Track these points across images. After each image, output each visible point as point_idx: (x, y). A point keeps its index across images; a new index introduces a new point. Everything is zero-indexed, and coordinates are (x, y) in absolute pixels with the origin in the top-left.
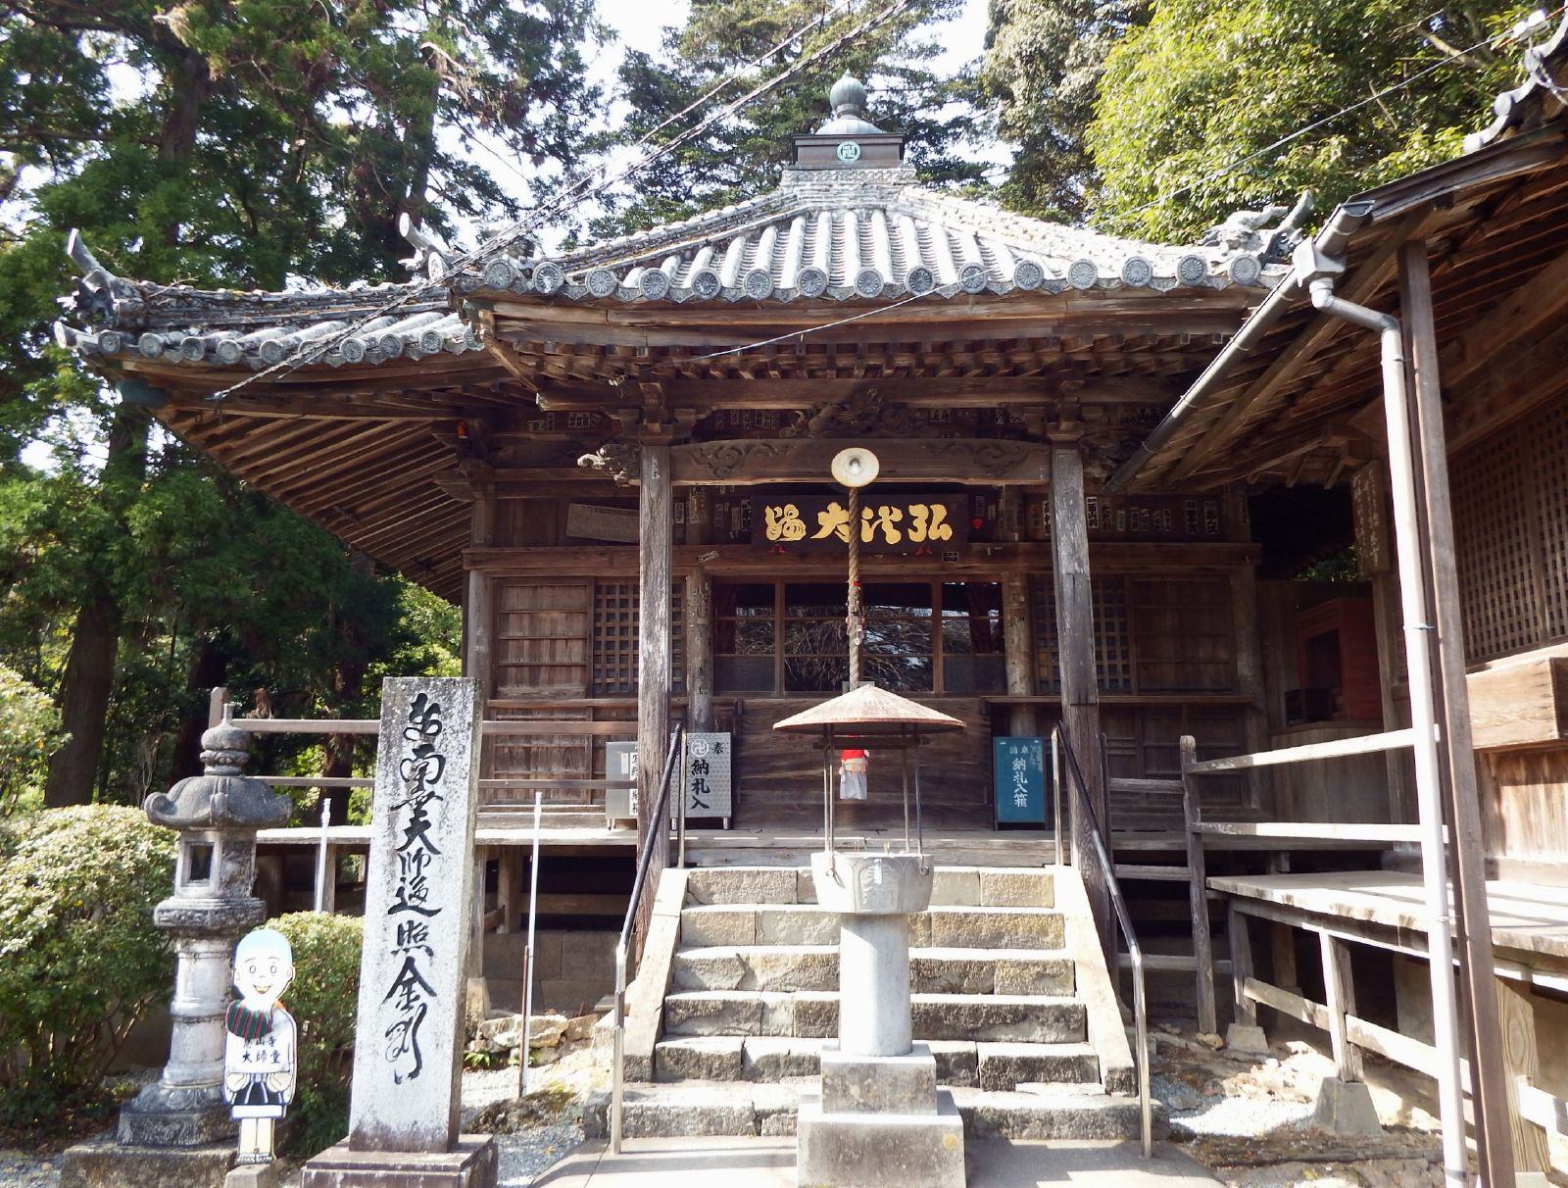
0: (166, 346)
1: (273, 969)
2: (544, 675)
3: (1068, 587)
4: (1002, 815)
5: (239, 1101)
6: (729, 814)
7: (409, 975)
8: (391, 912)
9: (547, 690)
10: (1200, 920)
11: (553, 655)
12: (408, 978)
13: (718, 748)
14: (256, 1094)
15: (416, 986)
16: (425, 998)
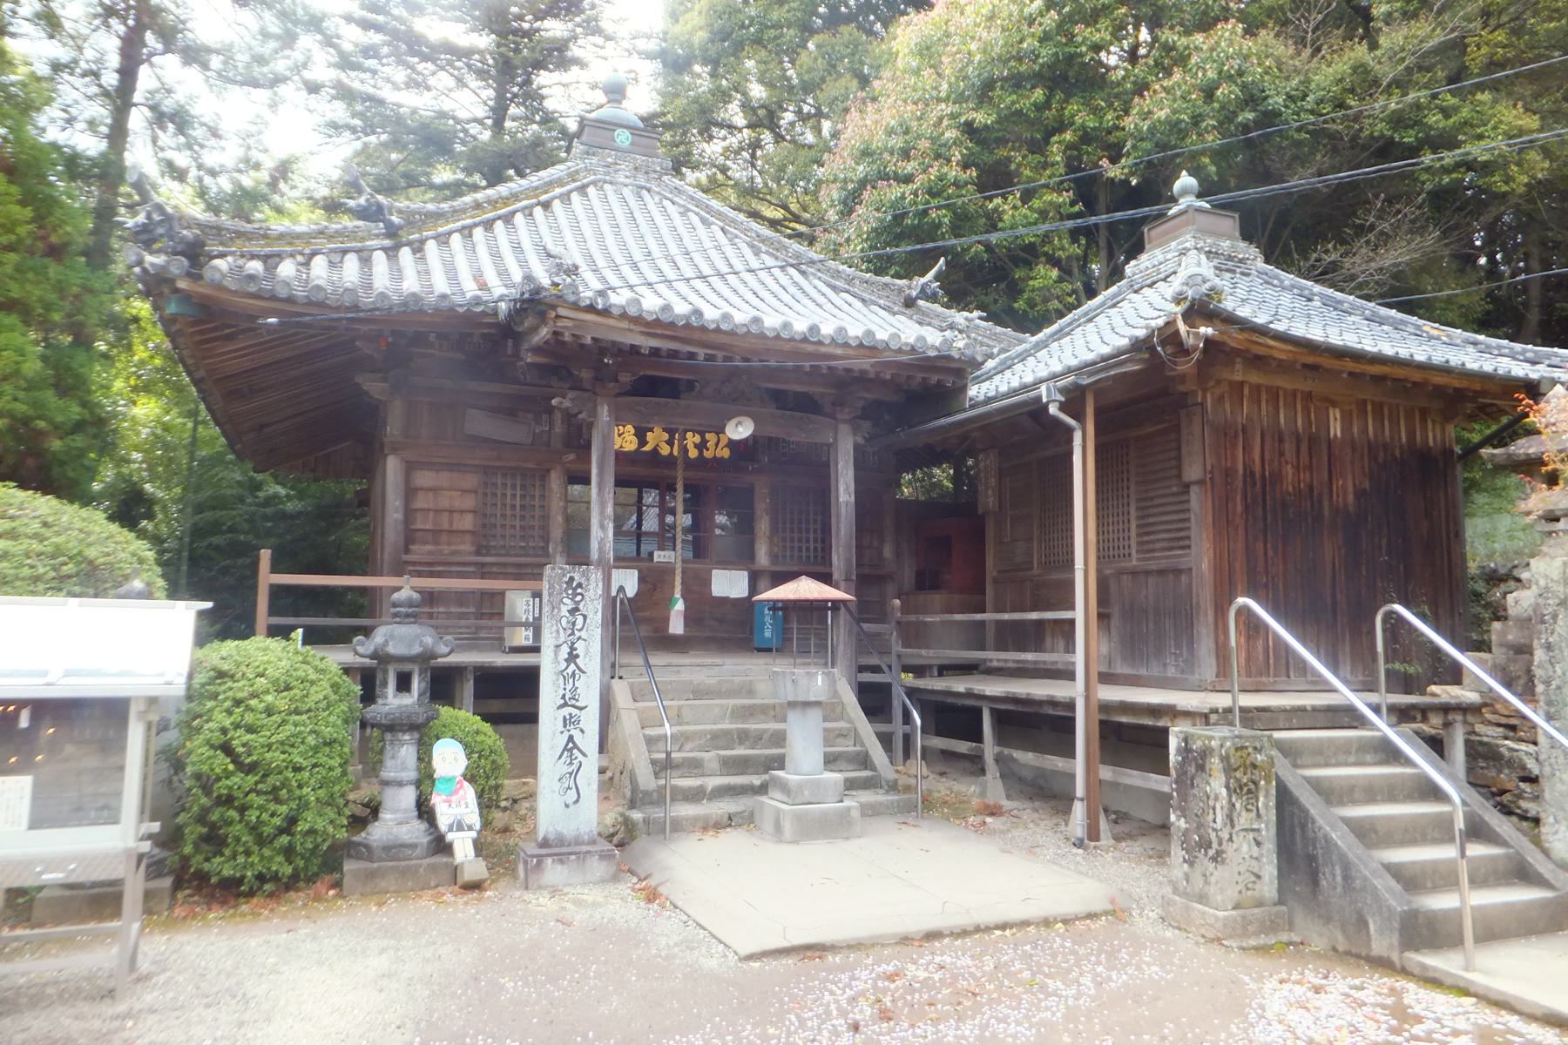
2: (444, 538)
3: (843, 510)
4: (757, 643)
5: (450, 830)
9: (446, 549)
11: (451, 523)
12: (571, 746)
14: (460, 826)
16: (581, 758)
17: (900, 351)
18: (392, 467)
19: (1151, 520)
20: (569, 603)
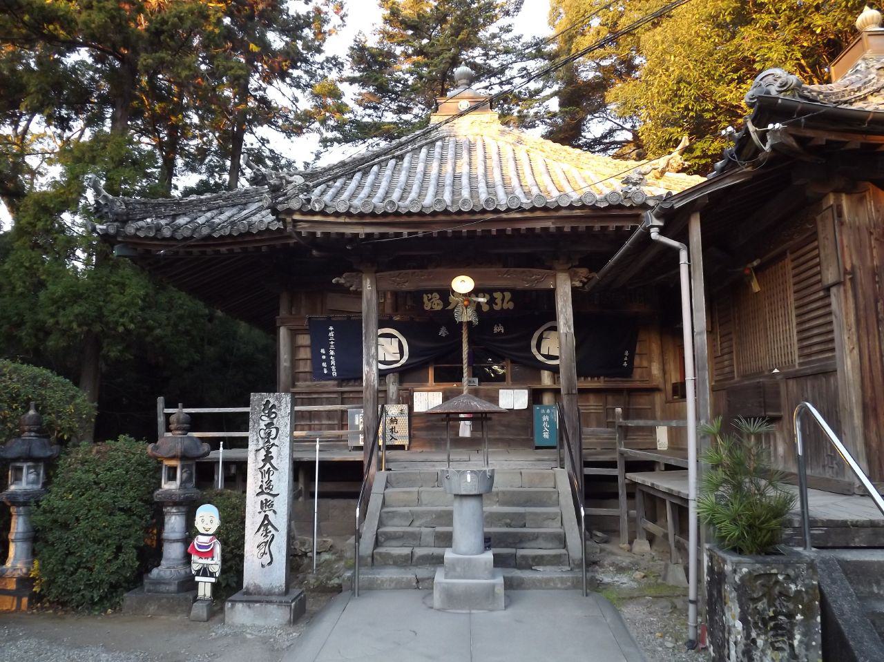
0: (137, 230)
1: (211, 522)
5: (198, 575)
6: (407, 443)
7: (266, 522)
8: (257, 495)
10: (622, 492)
13: (402, 412)
14: (205, 572)
15: (269, 527)
16: (273, 532)
17: (571, 207)
18: (283, 332)
19: (807, 325)
20: (267, 420)
